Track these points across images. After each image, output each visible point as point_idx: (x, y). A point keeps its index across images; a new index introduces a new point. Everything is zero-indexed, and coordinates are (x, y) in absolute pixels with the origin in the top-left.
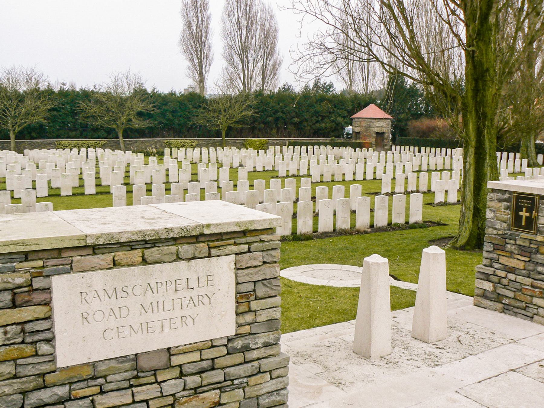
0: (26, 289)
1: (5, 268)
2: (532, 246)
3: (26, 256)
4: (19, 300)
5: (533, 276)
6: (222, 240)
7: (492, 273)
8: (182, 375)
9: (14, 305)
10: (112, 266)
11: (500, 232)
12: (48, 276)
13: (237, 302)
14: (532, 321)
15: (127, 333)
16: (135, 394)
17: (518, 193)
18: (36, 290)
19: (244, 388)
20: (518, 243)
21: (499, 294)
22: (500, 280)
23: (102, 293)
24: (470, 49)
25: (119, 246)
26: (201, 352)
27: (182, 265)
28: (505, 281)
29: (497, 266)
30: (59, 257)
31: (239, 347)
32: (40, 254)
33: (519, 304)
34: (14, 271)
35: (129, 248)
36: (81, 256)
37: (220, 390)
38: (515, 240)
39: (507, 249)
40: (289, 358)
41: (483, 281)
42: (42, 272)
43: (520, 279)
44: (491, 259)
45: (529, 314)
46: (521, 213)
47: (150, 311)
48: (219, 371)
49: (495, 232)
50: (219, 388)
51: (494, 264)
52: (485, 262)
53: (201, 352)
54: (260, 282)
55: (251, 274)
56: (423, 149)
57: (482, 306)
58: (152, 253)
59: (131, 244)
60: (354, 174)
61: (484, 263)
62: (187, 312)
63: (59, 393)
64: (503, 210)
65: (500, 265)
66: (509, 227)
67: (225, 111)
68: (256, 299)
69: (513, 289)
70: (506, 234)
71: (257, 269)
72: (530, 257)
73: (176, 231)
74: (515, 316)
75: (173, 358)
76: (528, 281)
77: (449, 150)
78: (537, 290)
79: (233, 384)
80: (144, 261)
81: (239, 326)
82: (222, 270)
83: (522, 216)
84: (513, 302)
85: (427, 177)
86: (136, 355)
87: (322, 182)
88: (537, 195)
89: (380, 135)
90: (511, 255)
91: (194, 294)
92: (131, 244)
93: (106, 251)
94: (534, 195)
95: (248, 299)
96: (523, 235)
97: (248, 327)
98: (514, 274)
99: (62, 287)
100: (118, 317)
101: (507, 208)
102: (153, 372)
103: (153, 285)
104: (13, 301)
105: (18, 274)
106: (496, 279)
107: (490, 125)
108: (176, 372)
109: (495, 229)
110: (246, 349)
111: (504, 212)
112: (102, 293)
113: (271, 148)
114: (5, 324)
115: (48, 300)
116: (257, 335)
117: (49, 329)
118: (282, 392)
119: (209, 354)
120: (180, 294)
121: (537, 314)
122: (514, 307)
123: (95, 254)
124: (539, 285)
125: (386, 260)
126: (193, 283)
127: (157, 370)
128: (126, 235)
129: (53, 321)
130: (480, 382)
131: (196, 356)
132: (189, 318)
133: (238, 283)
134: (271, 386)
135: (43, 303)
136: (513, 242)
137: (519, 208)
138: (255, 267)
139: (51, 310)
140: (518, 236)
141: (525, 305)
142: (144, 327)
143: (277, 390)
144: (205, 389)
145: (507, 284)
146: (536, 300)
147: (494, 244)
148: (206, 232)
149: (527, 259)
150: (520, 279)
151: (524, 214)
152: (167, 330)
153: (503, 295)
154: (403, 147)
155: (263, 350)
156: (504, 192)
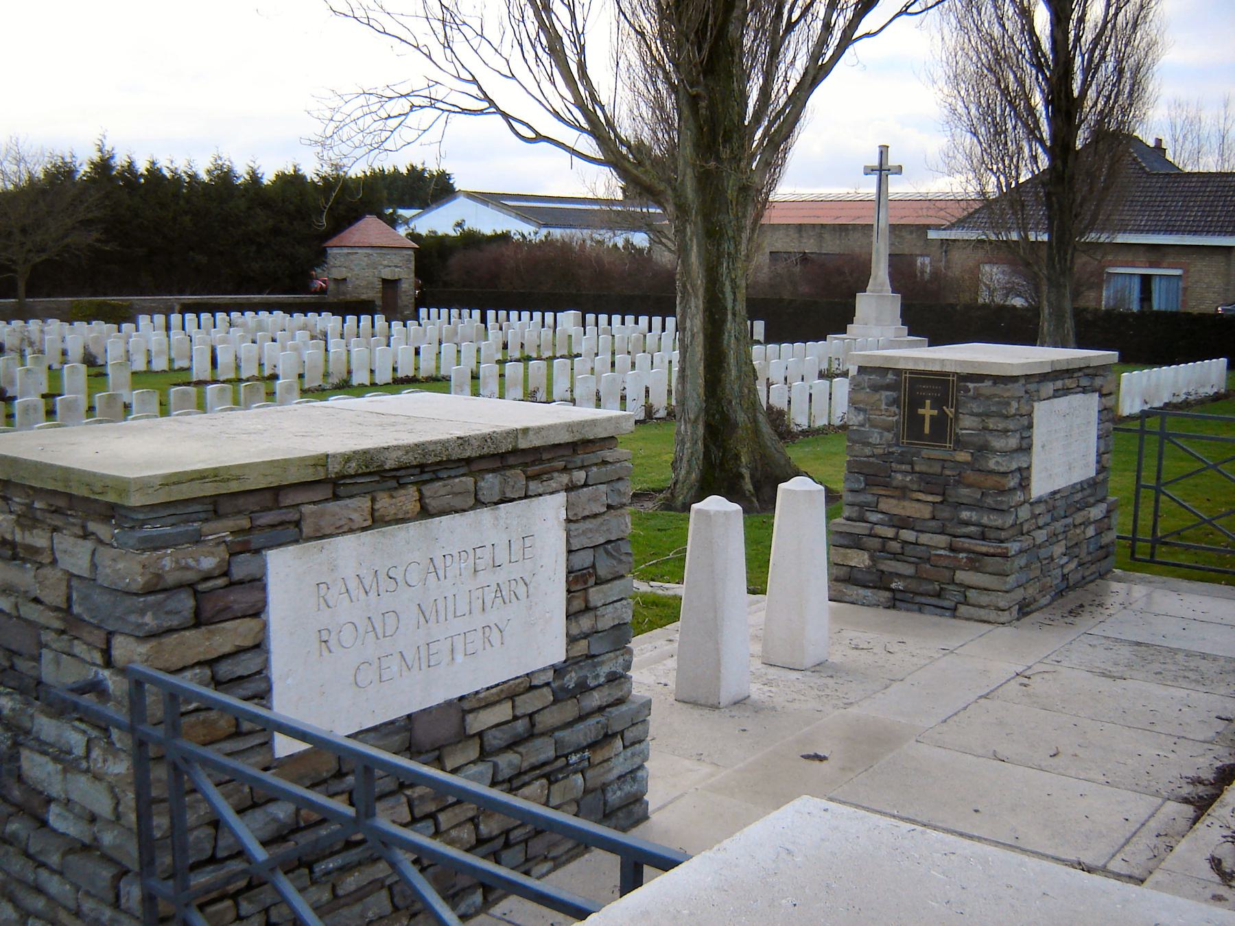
0: (221, 582)
1: (179, 534)
2: (947, 472)
3: (215, 507)
4: (208, 609)
5: (951, 531)
6: (541, 461)
7: (867, 532)
8: (484, 755)
9: (199, 621)
10: (369, 523)
11: (879, 451)
12: (257, 551)
13: (569, 591)
14: (954, 617)
15: (395, 668)
16: (416, 802)
17: (912, 372)
18: (241, 582)
19: (582, 772)
20: (917, 468)
21: (883, 572)
22: (884, 545)
23: (353, 584)
24: (693, 91)
25: (377, 478)
26: (513, 702)
27: (485, 514)
28: (895, 546)
29: (874, 517)
30: (276, 506)
31: (572, 685)
32: (241, 501)
33: (929, 587)
34: (197, 542)
35: (394, 483)
36: (314, 503)
37: (549, 780)
38: (912, 464)
39: (895, 483)
40: (650, 701)
41: (849, 551)
42: (247, 542)
43: (925, 538)
44: (861, 506)
45: (946, 604)
46: (921, 411)
47: (433, 618)
48: (546, 739)
49: (867, 451)
50: (543, 776)
51: (868, 514)
52: (847, 512)
53: (513, 702)
54: (601, 549)
55: (591, 530)
56: (491, 314)
57: (847, 599)
58: (436, 492)
59: (398, 474)
60: (372, 371)
61: (846, 514)
62: (493, 617)
63: (281, 815)
64: (884, 407)
65: (880, 516)
66: (898, 439)
67: (24, 231)
68: (596, 584)
69: (913, 559)
70: (893, 453)
71: (600, 520)
72: (944, 494)
73: (476, 444)
74: (920, 611)
75: (470, 718)
76: (942, 540)
77: (549, 316)
78: (961, 555)
79: (568, 764)
80: (425, 513)
81: (571, 640)
82: (544, 519)
83: (923, 416)
84: (913, 585)
85: (544, 370)
86: (409, 716)
87: (373, 384)
88: (954, 374)
89: (390, 285)
90: (903, 493)
91: (501, 576)
92: (398, 474)
93: (355, 490)
94: (947, 374)
95: (585, 582)
96: (926, 453)
97: (584, 643)
98: (913, 529)
99: (286, 571)
100: (380, 635)
101: (895, 402)
102: (437, 753)
103: (439, 562)
104: (197, 612)
105: (205, 549)
106: (875, 543)
107: (732, 250)
108: (474, 753)
109: (869, 444)
110: (583, 688)
111: (886, 410)
112: (353, 584)
113: (144, 320)
114: (180, 665)
115: (260, 605)
116: (599, 659)
117: (260, 672)
118: (640, 773)
119: (528, 704)
120: (483, 578)
121: (966, 602)
122: (916, 594)
123: (336, 497)
124: (966, 545)
125: (736, 507)
126: (502, 556)
127: (443, 746)
128: (394, 455)
129: (267, 652)
130: (945, 721)
131: (503, 712)
132: (495, 630)
133: (569, 552)
134: (619, 766)
135: (251, 612)
136: (908, 468)
137: (915, 403)
138: (595, 516)
139: (265, 626)
140: (918, 454)
141: (938, 588)
142: (424, 653)
143: (631, 772)
144: (526, 778)
145: (899, 551)
146: (961, 576)
147: (866, 475)
148: (523, 444)
149: (938, 499)
150: (925, 538)
151: (928, 412)
152: (459, 657)
153: (891, 573)
154: (454, 312)
155: (606, 690)
156: (883, 371)
